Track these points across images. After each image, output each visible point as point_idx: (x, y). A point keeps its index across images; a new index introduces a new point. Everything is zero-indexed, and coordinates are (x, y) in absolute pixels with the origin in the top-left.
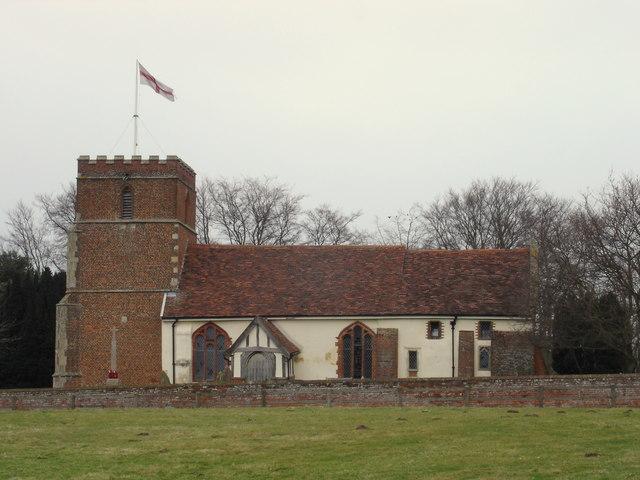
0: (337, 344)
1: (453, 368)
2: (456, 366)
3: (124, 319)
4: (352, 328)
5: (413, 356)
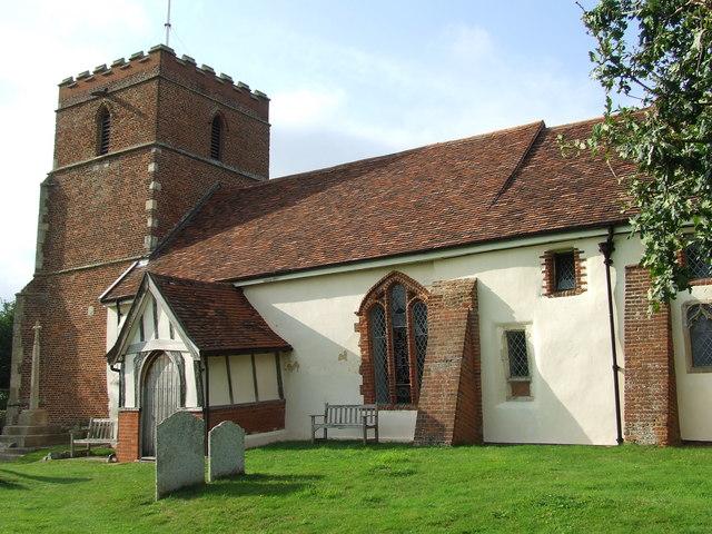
0: (358, 328)
1: (616, 368)
2: (621, 363)
3: (91, 309)
4: (384, 288)
5: (517, 343)
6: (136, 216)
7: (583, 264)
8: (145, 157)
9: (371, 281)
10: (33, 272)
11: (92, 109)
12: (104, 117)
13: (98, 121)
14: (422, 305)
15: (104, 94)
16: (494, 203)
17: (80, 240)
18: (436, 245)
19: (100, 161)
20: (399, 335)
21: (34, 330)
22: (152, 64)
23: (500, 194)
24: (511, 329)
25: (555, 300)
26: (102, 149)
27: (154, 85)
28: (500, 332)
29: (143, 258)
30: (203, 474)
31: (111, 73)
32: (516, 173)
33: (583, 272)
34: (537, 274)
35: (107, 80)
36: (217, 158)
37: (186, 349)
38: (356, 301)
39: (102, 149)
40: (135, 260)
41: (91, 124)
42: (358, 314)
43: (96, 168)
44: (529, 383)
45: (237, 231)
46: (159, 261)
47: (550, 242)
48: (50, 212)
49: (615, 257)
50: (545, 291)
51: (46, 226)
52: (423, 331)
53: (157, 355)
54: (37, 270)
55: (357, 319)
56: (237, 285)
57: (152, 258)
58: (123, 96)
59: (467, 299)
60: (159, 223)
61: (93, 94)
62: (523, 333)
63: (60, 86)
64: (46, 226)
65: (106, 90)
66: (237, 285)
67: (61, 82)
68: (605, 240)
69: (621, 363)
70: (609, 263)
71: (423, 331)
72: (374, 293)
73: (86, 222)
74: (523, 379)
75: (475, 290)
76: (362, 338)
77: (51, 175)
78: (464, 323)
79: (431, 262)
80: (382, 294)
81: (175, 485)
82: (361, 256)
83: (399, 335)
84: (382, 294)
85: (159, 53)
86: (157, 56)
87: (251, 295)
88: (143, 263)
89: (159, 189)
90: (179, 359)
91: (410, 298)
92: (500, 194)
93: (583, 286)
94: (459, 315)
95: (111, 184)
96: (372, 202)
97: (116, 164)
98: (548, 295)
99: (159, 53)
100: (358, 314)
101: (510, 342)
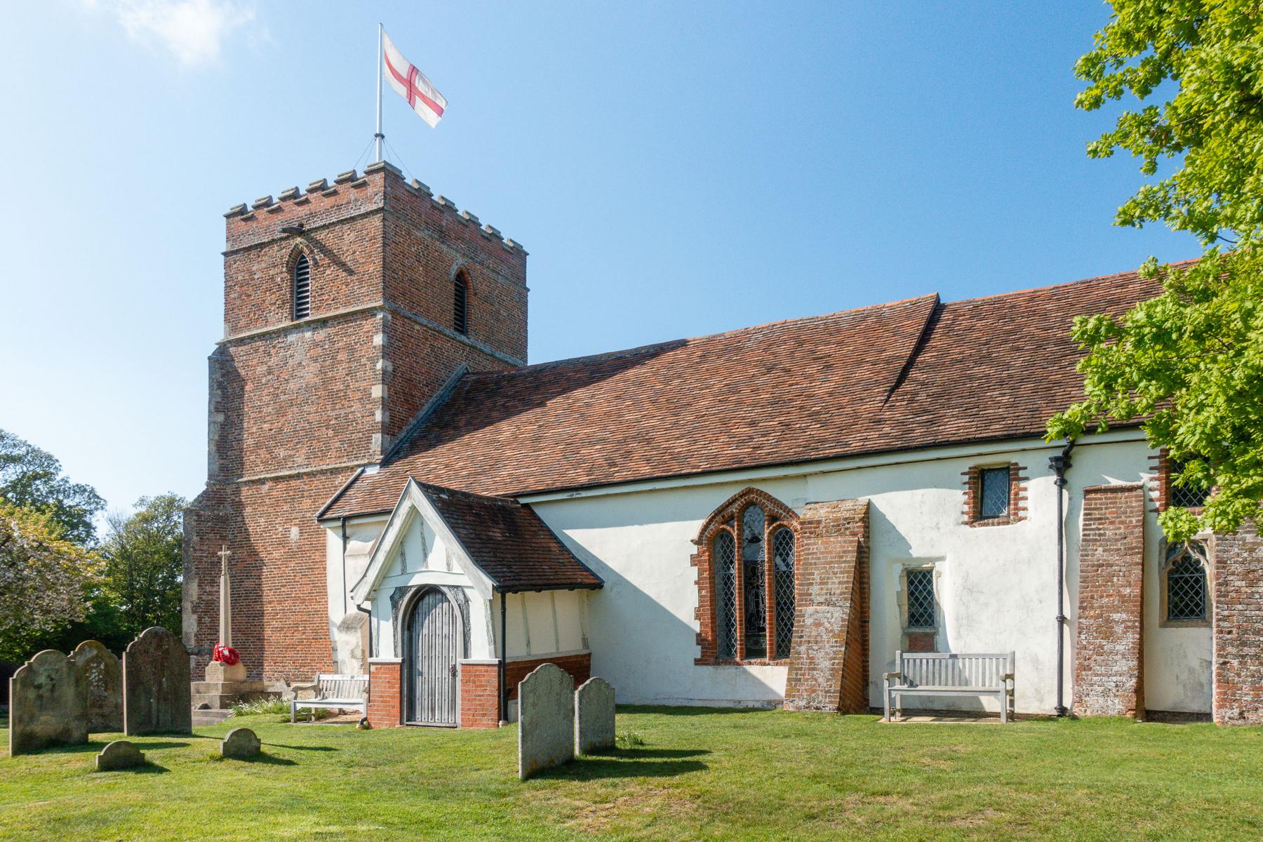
0: (695, 560)
1: (1062, 620)
3: (295, 531)
4: (734, 509)
6: (357, 406)
7: (1023, 484)
8: (368, 325)
9: (719, 498)
10: (206, 479)
11: (281, 253)
12: (298, 267)
13: (290, 271)
14: (787, 532)
15: (299, 231)
16: (887, 401)
17: (273, 438)
18: (813, 455)
19: (297, 328)
20: (751, 571)
21: (220, 558)
22: (370, 190)
23: (892, 390)
24: (913, 565)
25: (980, 531)
26: (298, 309)
27: (377, 221)
28: (898, 569)
29: (370, 464)
30: (573, 750)
31: (279, 210)
32: (911, 362)
33: (1022, 494)
34: (958, 499)
35: (303, 211)
36: (462, 332)
37: (470, 584)
38: (694, 528)
39: (298, 309)
40: (359, 466)
41: (282, 276)
42: (698, 542)
43: (292, 338)
44: (934, 634)
45: (506, 428)
46: (393, 468)
47: (980, 455)
48: (225, 396)
49: (1070, 475)
50: (966, 518)
51: (220, 418)
52: (787, 565)
53: (428, 592)
54: (210, 477)
55: (694, 550)
56: (523, 501)
57: (385, 463)
58: (321, 236)
59: (858, 527)
60: (392, 417)
61: (284, 231)
62: (930, 571)
63: (228, 216)
64: (220, 418)
65: (302, 225)
66: (523, 501)
67: (228, 211)
68: (1059, 453)
69: (1067, 613)
70: (1062, 483)
71: (787, 565)
72: (722, 515)
73: (281, 412)
74: (928, 630)
75: (869, 516)
76: (700, 574)
77: (223, 349)
78: (852, 557)
79: (805, 476)
80: (732, 517)
81: (542, 759)
82: (704, 466)
83: (751, 571)
84: (732, 517)
85: (382, 174)
86: (379, 178)
87: (540, 512)
88: (372, 471)
89: (390, 369)
90: (461, 597)
91: (769, 525)
92: (892, 390)
93: (1021, 514)
94: (843, 547)
95: (316, 361)
96: (703, 397)
97: (322, 334)
98: (970, 524)
99: (382, 174)
100: (698, 542)
101: (911, 583)
